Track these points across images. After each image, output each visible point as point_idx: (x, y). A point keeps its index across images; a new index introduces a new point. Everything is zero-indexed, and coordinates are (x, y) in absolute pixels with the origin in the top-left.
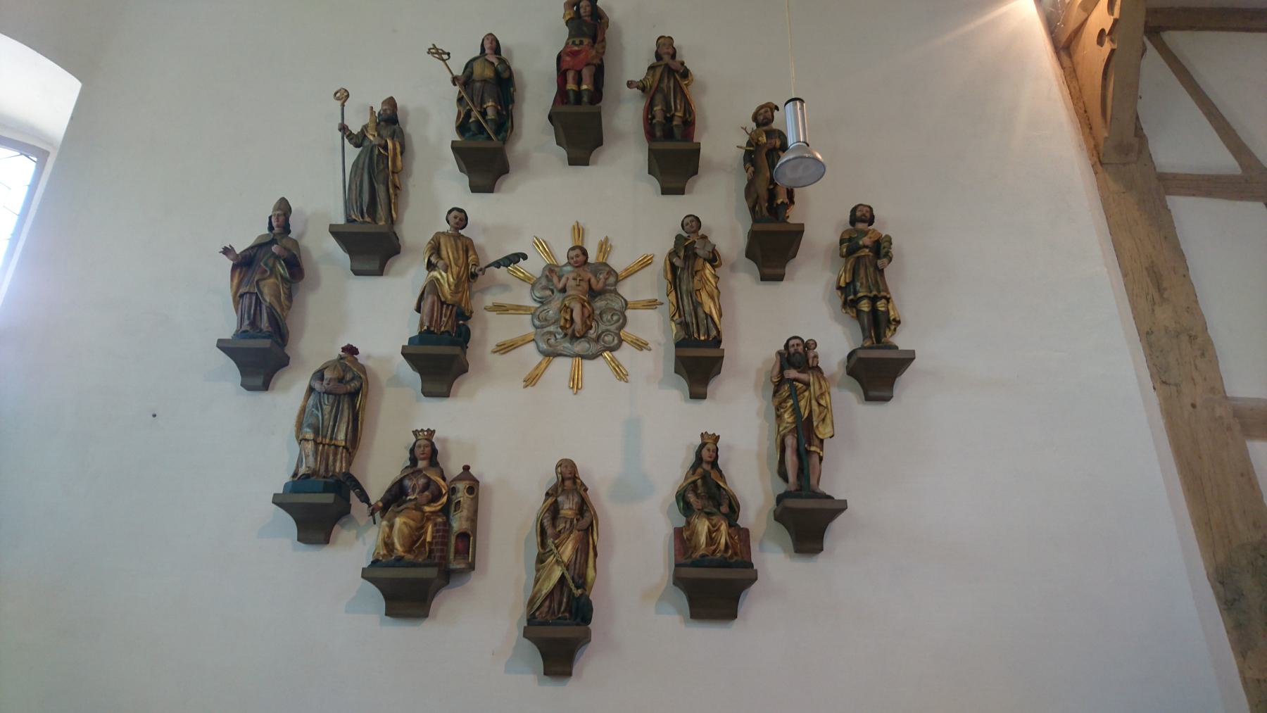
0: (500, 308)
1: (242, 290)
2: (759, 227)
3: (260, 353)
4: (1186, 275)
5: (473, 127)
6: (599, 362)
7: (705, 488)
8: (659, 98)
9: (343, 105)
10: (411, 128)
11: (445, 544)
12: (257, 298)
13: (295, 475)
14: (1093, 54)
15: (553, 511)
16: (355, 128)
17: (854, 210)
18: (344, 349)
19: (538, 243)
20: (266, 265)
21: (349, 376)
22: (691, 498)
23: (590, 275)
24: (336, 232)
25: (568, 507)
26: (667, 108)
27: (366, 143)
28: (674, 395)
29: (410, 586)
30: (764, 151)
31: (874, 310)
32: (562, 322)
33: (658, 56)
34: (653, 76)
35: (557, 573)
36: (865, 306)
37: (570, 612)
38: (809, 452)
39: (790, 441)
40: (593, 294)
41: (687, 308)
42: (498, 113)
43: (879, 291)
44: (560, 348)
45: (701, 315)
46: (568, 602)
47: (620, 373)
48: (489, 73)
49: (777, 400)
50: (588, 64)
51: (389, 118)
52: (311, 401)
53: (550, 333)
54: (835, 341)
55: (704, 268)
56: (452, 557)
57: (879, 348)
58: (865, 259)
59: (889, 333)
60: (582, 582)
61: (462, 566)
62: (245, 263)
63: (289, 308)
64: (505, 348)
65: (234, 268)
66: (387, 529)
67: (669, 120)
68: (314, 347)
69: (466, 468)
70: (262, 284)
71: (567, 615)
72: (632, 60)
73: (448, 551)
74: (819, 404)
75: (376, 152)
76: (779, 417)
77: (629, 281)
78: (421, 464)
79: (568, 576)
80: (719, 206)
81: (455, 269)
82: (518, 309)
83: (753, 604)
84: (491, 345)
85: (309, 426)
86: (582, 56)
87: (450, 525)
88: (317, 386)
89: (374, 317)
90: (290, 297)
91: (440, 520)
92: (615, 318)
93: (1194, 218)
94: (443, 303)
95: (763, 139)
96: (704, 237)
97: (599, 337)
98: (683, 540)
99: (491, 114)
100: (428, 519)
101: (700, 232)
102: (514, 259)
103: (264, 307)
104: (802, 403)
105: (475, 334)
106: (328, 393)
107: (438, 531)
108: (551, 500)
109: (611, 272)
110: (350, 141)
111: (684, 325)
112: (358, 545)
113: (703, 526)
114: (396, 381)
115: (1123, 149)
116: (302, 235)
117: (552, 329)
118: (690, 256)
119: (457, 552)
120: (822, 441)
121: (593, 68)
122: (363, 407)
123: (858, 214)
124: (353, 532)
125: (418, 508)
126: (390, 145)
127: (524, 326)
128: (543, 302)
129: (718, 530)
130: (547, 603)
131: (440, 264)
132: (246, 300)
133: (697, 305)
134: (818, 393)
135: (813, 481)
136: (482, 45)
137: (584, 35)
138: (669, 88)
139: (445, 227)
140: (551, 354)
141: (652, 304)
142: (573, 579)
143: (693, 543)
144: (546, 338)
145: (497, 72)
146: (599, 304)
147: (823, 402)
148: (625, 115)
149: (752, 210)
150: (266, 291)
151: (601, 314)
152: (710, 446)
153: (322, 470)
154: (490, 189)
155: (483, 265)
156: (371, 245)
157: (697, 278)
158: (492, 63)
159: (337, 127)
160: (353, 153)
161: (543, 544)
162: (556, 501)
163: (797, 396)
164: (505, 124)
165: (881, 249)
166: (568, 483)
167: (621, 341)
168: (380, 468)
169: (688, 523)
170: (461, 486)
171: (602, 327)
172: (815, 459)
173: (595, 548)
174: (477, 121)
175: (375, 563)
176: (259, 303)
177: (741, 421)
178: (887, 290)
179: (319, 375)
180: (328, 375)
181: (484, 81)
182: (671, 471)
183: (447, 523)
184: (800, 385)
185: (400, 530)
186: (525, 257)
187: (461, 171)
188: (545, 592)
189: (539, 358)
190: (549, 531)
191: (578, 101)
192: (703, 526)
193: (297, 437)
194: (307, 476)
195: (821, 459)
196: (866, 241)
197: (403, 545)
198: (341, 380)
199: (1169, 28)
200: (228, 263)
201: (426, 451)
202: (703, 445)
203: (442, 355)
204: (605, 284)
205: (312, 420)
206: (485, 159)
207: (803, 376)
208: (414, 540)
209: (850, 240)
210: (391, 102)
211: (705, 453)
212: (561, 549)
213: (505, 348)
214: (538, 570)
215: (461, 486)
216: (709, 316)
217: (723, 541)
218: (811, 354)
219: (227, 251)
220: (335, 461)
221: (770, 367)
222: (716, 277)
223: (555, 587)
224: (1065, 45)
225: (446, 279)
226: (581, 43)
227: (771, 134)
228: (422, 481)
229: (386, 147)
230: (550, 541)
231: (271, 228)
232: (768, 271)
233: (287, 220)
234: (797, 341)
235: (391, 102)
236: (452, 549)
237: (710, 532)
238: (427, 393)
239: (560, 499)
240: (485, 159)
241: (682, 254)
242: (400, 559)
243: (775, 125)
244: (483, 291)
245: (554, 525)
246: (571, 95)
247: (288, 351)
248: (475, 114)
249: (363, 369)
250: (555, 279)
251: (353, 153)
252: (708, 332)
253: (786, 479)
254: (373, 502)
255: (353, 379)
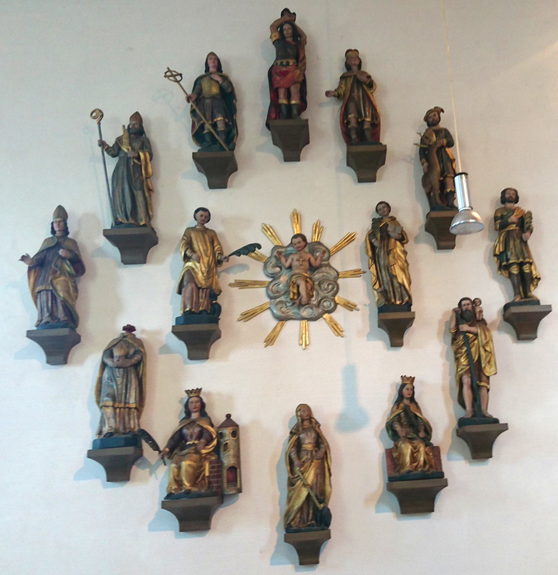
0: (242, 284)
1: (38, 289)
2: (435, 214)
3: (58, 337)
5: (208, 138)
6: (321, 322)
7: (406, 421)
8: (352, 106)
9: (99, 124)
10: (154, 134)
11: (220, 476)
12: (52, 295)
13: (100, 433)
15: (298, 446)
16: (111, 141)
17: (504, 192)
18: (125, 328)
19: (266, 229)
20: (56, 266)
21: (132, 351)
22: (398, 427)
23: (309, 256)
24: (108, 235)
25: (308, 443)
27: (122, 155)
28: (378, 346)
29: (196, 506)
31: (521, 272)
32: (291, 296)
33: (348, 66)
34: (346, 85)
35: (304, 493)
36: (515, 270)
37: (316, 520)
38: (479, 387)
39: (466, 380)
40: (313, 269)
41: (385, 279)
42: (226, 124)
43: (524, 258)
44: (291, 313)
46: (314, 513)
47: (337, 330)
48: (215, 90)
49: (455, 347)
50: (295, 83)
51: (137, 131)
52: (106, 375)
53: (281, 302)
54: (494, 297)
56: (225, 485)
57: (525, 303)
59: (532, 288)
61: (234, 492)
63: (76, 297)
64: (248, 316)
65: (30, 269)
66: (176, 470)
67: (361, 124)
68: (99, 329)
69: (229, 416)
71: (314, 522)
73: (222, 482)
74: (486, 351)
75: (132, 163)
76: (457, 359)
78: (194, 416)
79: (313, 495)
80: (400, 189)
81: (206, 259)
83: (444, 500)
84: (237, 315)
85: (108, 395)
86: (290, 75)
87: (222, 462)
88: (109, 362)
89: (142, 299)
90: (76, 289)
91: (213, 458)
92: (330, 287)
94: (199, 288)
97: (319, 303)
98: (393, 458)
100: (205, 459)
101: (391, 214)
103: (59, 301)
104: (473, 350)
105: (224, 307)
106: (119, 367)
108: (295, 438)
109: (327, 250)
110: (108, 153)
111: (384, 293)
112: (152, 483)
114: (165, 349)
116: (77, 234)
117: (283, 298)
118: (384, 234)
119: (229, 481)
121: (298, 85)
122: (144, 374)
123: (507, 196)
124: (148, 470)
125: (197, 452)
126: (142, 155)
127: (260, 296)
128: (274, 277)
129: (418, 451)
130: (298, 515)
132: (43, 296)
133: (393, 277)
134: (484, 342)
135: (483, 408)
136: (207, 64)
138: (359, 97)
139: (194, 223)
140: (282, 319)
141: (356, 273)
142: (316, 496)
143: (400, 462)
144: (279, 306)
145: (221, 88)
146: (317, 276)
147: (488, 349)
148: (324, 118)
149: (428, 195)
150: (59, 288)
151: (319, 284)
152: (408, 386)
154: (223, 185)
155: (226, 254)
156: (135, 240)
157: (391, 256)
158: (217, 82)
159: (97, 143)
160: (112, 163)
161: (292, 471)
162: (299, 438)
163: (469, 344)
164: (231, 134)
165: (525, 224)
167: (336, 304)
168: (162, 419)
169: (396, 446)
170: (227, 431)
171: (322, 294)
172: (484, 391)
173: (329, 470)
174: (210, 133)
175: (170, 496)
176: (54, 298)
177: (427, 361)
178: (530, 257)
179: (109, 352)
180: (117, 353)
181: (213, 98)
182: (378, 406)
184: (471, 335)
185: (186, 471)
186: (259, 247)
187: (199, 170)
188: (297, 506)
190: (296, 462)
191: (289, 115)
192: (407, 449)
193: (98, 402)
194: (110, 434)
195: (488, 390)
196: (513, 218)
197: (189, 482)
198: (127, 356)
200: (25, 267)
201: (196, 405)
202: (403, 386)
203: (200, 329)
204: (322, 260)
205: (109, 391)
206: (217, 162)
207: (473, 329)
208: (196, 476)
209: (502, 217)
210: (137, 117)
211: (405, 391)
212: (306, 475)
213: (248, 316)
214: (290, 491)
215: (227, 431)
216: (402, 285)
217: (422, 459)
218: (478, 310)
219: (24, 258)
220: (129, 420)
221: (448, 318)
222: (405, 253)
223: (304, 503)
225: (200, 269)
226: (288, 64)
227: (438, 132)
228: (197, 430)
229: (138, 158)
230: (297, 469)
231: (53, 232)
232: (442, 244)
233: (66, 224)
234: (467, 302)
235: (137, 117)
236: (225, 480)
238: (191, 357)
239: (302, 436)
240: (217, 162)
241: (378, 236)
242: (188, 492)
243: (442, 125)
244: (227, 270)
246: (284, 109)
248: (208, 127)
249: (140, 343)
250: (283, 260)
251: (112, 163)
252: (402, 299)
254: (162, 448)
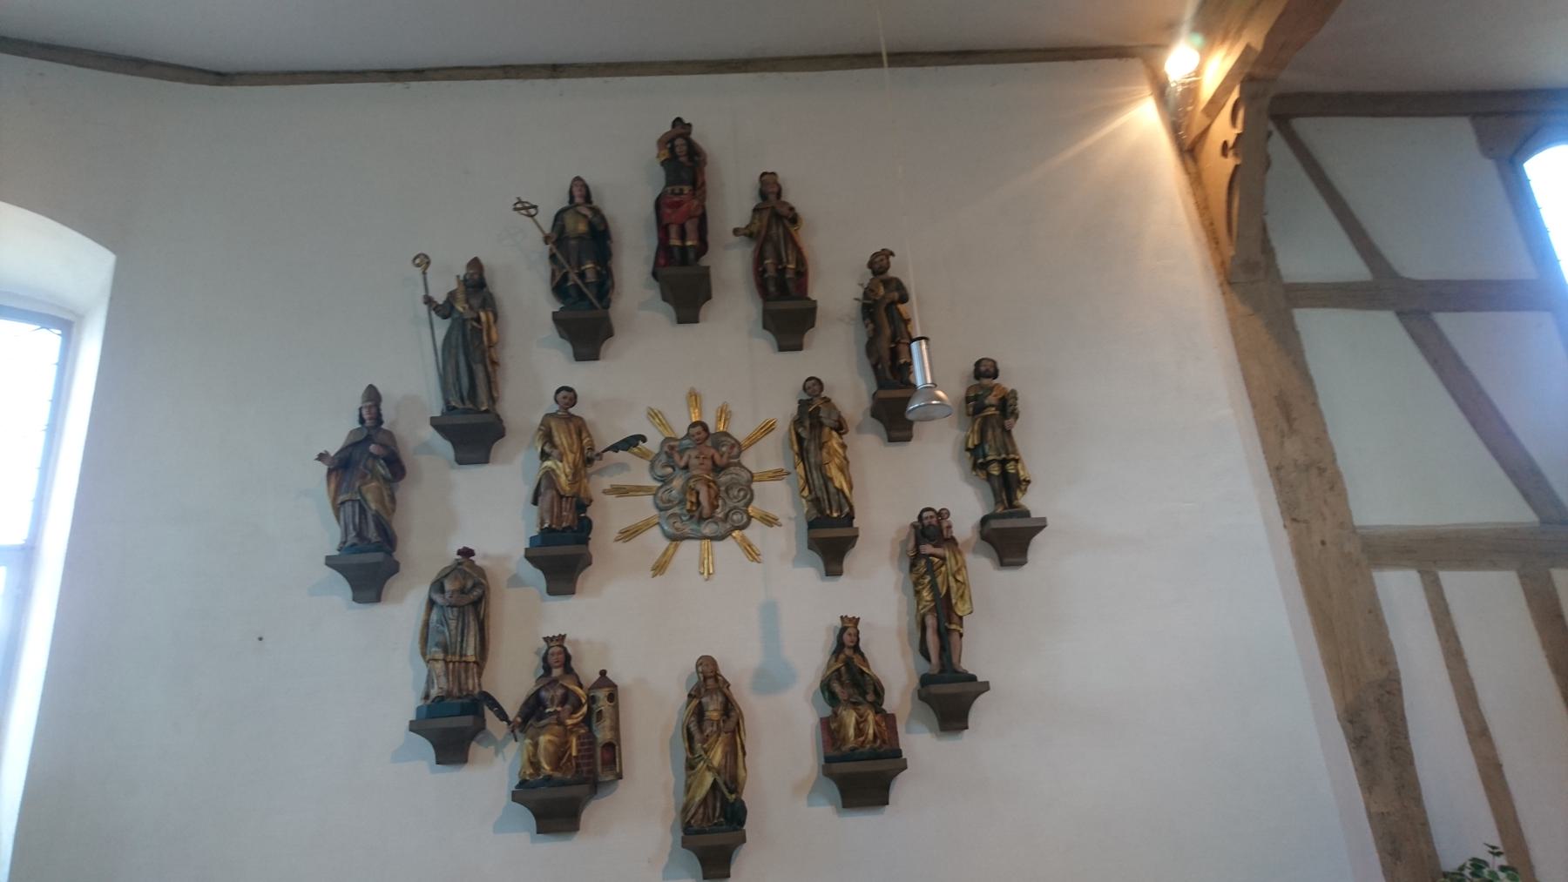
0: (621, 491)
1: (341, 498)
2: (885, 394)
3: (368, 564)
4: (1315, 404)
5: (573, 292)
6: (729, 540)
7: (848, 677)
8: (769, 248)
10: (499, 286)
11: (592, 756)
13: (427, 697)
14: (1220, 167)
15: (699, 713)
16: (440, 298)
17: (978, 364)
18: (460, 553)
19: (653, 415)
21: (470, 584)
22: (837, 687)
23: (713, 451)
24: (437, 424)
25: (713, 709)
26: (779, 260)
28: (809, 575)
29: (559, 800)
30: (883, 307)
31: (1004, 473)
36: (995, 470)
38: (949, 631)
39: (931, 621)
40: (717, 469)
42: (598, 273)
45: (832, 490)
47: (751, 552)
48: (582, 227)
51: (476, 283)
52: (434, 616)
54: (967, 507)
55: (831, 436)
57: (1011, 516)
58: (990, 412)
59: (1019, 494)
60: (735, 784)
62: (343, 466)
64: (629, 534)
65: (330, 472)
68: (424, 554)
69: (603, 673)
70: (364, 488)
72: (732, 204)
76: (917, 593)
77: (752, 450)
78: (556, 672)
79: (720, 782)
80: (836, 360)
81: (571, 457)
82: (638, 490)
83: (903, 789)
84: (614, 533)
85: (437, 645)
86: (684, 208)
88: (438, 598)
89: (484, 512)
90: (393, 499)
93: (1320, 329)
94: (561, 497)
95: (882, 291)
96: (827, 400)
97: (727, 515)
98: (830, 731)
99: (591, 277)
100: (571, 732)
102: (631, 443)
104: (940, 580)
106: (452, 606)
107: (582, 744)
108: (695, 702)
111: (816, 502)
113: (850, 718)
115: (1249, 267)
117: (676, 510)
118: (814, 421)
119: (604, 763)
120: (961, 618)
121: (696, 221)
123: (983, 369)
126: (482, 315)
127: (644, 508)
128: (666, 481)
131: (555, 453)
133: (827, 480)
135: (955, 660)
137: (683, 182)
139: (555, 408)
140: (676, 538)
141: (777, 475)
145: (591, 224)
146: (724, 479)
148: (731, 265)
149: (875, 367)
150: (369, 497)
151: (727, 491)
152: (850, 630)
153: (456, 690)
154: (594, 357)
155: (599, 449)
156: (473, 432)
160: (442, 327)
161: (691, 749)
164: (604, 286)
165: (1007, 407)
166: (710, 682)
167: (750, 518)
168: (511, 677)
169: (835, 714)
170: (602, 694)
171: (731, 504)
172: (955, 636)
174: (576, 285)
175: (523, 784)
176: (363, 511)
177: (877, 595)
178: (1015, 452)
179: (438, 586)
180: (448, 586)
181: (580, 237)
182: (810, 659)
183: (590, 734)
188: (698, 799)
189: (666, 543)
190: (697, 736)
192: (850, 718)
193: (424, 655)
194: (440, 699)
196: (992, 399)
198: (462, 591)
199: (1298, 115)
200: (323, 469)
201: (557, 657)
202: (843, 629)
203: (563, 552)
205: (439, 638)
206: (586, 324)
207: (939, 551)
209: (976, 398)
210: (475, 264)
211: (846, 638)
213: (629, 534)
215: (602, 694)
216: (840, 491)
217: (871, 731)
218: (945, 524)
222: (844, 446)
224: (1189, 150)
228: (560, 692)
229: (478, 320)
230: (698, 746)
231: (362, 421)
232: (896, 434)
233: (379, 410)
235: (475, 264)
236: (599, 762)
237: (858, 723)
239: (704, 700)
240: (586, 324)
241: (807, 423)
242: (549, 778)
243: (892, 273)
244: (599, 472)
245: (701, 731)
246: (676, 253)
247: (397, 555)
248: (573, 278)
249: (481, 572)
250: (677, 457)
251: (442, 327)
252: (840, 509)
253: (928, 658)
255: (474, 586)
